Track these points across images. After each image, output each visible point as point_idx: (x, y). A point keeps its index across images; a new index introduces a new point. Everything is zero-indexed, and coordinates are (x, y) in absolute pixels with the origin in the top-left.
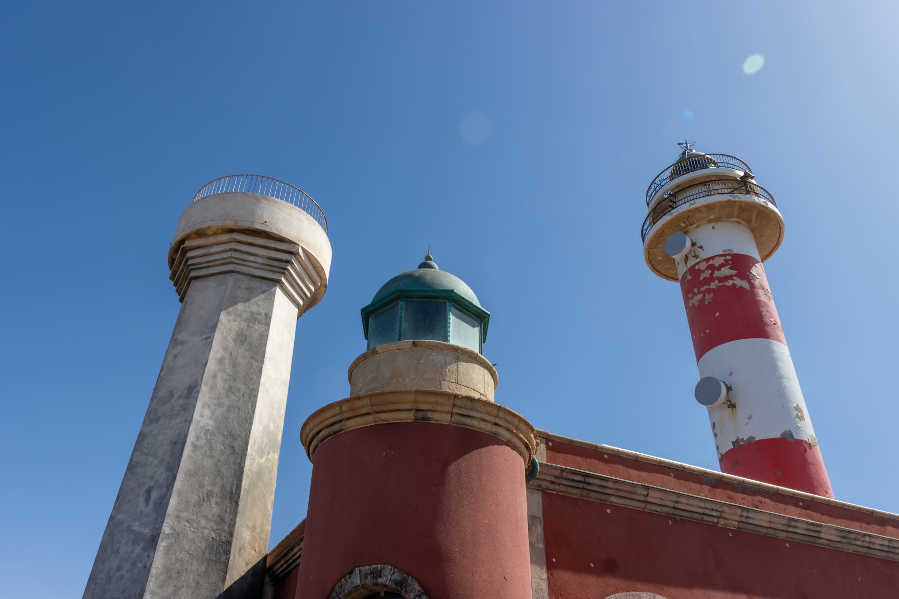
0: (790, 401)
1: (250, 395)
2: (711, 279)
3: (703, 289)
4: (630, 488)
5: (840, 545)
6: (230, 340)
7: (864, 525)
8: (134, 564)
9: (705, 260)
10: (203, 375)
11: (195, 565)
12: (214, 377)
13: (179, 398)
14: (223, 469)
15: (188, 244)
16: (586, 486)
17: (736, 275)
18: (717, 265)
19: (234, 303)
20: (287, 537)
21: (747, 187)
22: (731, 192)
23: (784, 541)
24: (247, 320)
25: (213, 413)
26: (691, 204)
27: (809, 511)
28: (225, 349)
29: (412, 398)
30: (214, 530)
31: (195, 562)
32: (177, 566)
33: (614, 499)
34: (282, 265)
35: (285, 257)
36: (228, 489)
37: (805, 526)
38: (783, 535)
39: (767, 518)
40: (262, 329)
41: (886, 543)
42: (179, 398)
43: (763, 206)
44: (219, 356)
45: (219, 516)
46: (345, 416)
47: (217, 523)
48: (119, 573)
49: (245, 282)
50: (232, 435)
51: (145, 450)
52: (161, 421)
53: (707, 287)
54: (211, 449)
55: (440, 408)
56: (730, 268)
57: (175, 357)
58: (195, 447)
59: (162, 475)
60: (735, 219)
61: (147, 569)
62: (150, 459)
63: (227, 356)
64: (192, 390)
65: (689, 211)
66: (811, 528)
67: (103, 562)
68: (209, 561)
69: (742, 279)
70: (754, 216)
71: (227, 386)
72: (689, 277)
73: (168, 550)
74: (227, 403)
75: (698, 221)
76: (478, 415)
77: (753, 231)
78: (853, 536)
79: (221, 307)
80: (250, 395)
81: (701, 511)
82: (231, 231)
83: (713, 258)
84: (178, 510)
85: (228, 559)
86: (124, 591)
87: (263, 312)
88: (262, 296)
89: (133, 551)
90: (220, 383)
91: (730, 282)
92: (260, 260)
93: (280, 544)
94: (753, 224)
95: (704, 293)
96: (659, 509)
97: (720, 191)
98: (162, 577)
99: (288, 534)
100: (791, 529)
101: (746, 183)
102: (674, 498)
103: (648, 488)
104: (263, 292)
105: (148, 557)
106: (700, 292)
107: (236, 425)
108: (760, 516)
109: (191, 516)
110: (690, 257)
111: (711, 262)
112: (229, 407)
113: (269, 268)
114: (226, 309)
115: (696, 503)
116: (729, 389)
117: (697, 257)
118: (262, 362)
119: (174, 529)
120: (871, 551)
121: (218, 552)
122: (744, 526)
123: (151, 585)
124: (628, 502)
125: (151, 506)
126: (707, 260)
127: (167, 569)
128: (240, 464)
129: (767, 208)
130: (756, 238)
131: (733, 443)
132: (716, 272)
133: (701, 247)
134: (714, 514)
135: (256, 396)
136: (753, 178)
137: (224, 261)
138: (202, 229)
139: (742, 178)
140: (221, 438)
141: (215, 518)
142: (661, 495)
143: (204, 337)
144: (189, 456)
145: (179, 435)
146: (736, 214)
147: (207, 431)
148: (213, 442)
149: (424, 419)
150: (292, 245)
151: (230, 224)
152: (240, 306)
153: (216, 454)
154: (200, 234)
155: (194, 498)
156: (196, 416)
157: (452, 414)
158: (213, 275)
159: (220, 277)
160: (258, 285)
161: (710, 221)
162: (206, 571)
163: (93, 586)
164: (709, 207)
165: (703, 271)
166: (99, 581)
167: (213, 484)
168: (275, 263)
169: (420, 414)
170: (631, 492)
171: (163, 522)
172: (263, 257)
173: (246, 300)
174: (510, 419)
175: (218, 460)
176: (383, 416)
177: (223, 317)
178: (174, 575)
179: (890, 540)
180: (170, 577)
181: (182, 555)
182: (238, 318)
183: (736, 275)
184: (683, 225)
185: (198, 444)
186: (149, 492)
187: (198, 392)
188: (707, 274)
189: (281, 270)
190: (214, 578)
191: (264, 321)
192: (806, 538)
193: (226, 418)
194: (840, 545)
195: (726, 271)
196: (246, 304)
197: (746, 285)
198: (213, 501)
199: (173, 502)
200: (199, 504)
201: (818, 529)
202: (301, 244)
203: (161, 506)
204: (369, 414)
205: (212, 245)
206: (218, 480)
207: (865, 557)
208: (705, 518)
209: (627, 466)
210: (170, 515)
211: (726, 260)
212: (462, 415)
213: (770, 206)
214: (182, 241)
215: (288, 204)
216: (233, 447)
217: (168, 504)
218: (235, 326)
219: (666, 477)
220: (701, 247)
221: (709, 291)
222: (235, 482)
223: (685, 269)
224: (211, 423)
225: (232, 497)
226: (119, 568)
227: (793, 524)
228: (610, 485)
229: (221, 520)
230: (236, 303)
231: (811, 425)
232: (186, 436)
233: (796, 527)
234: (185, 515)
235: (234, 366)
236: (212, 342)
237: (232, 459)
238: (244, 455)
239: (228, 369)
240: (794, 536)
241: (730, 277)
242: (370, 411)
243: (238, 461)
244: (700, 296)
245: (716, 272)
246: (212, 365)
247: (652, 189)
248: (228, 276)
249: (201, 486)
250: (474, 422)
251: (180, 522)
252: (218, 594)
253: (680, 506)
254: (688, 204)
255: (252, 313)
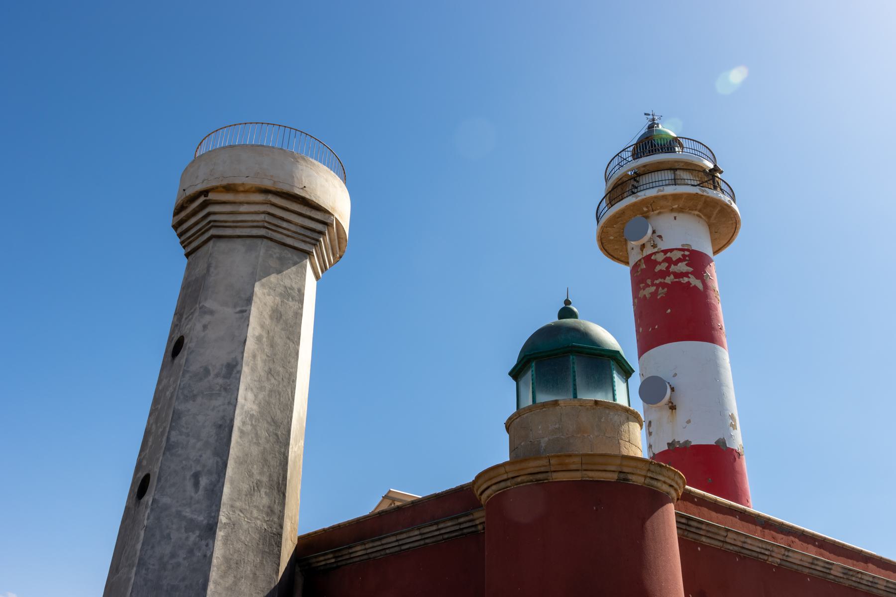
0: (727, 410)
1: (289, 379)
2: (664, 274)
3: (657, 282)
4: (716, 530)
5: (841, 580)
6: (267, 316)
7: (855, 562)
8: (191, 552)
9: (663, 251)
10: (243, 353)
11: (251, 557)
12: (254, 357)
13: (217, 375)
14: (269, 458)
15: (212, 196)
16: (688, 528)
17: (692, 273)
18: (674, 259)
19: (267, 274)
20: (324, 530)
21: (714, 182)
22: (698, 185)
23: (807, 576)
24: (281, 295)
25: (256, 396)
26: (659, 191)
27: (822, 550)
28: (262, 327)
29: (618, 462)
30: (266, 521)
31: (251, 553)
32: (236, 556)
33: (704, 539)
34: (315, 235)
35: (319, 227)
36: (275, 479)
37: (885, 584)
38: (806, 571)
39: (799, 557)
40: (296, 307)
41: (871, 579)
42: (217, 375)
43: (727, 205)
44: (257, 334)
45: (269, 507)
46: (553, 469)
47: (268, 515)
48: (173, 561)
49: (277, 250)
50: (274, 422)
51: (184, 430)
52: (199, 400)
53: (662, 280)
54: (257, 436)
55: (638, 472)
56: (687, 265)
57: (205, 327)
58: (242, 432)
59: (208, 458)
60: (697, 213)
61: (207, 559)
62: (192, 441)
63: (265, 334)
64: (232, 370)
65: (656, 197)
66: (827, 566)
67: (153, 547)
68: (263, 552)
69: (697, 278)
70: (715, 213)
71: (266, 369)
72: (644, 266)
73: (226, 539)
74: (268, 386)
75: (661, 208)
76: (663, 479)
77: (710, 226)
78: (851, 573)
79: (254, 278)
80: (289, 379)
81: (758, 550)
82: (266, 191)
83: (671, 250)
84: (232, 499)
85: (280, 551)
86: (183, 579)
87: (295, 286)
88: (294, 269)
89: (187, 538)
90: (260, 364)
91: (686, 280)
92: (293, 228)
93: (309, 535)
94: (712, 220)
95: (658, 286)
96: (731, 548)
97: (689, 182)
98: (223, 568)
99: (326, 526)
100: (813, 567)
101: (714, 177)
102: (743, 539)
103: (728, 530)
104: (295, 264)
105: (207, 545)
106: (653, 285)
107: (278, 412)
108: (796, 556)
109: (244, 506)
110: (648, 246)
111: (669, 255)
112: (271, 391)
113: (301, 237)
114: (260, 280)
115: (757, 544)
116: (673, 389)
117: (654, 246)
118: (298, 344)
119: (230, 519)
120: (860, 586)
121: (270, 544)
122: (784, 563)
123: (214, 575)
124: (713, 542)
125: (201, 492)
126: (665, 252)
127: (227, 560)
128: (284, 454)
129: (730, 207)
130: (711, 233)
131: (668, 444)
132: (673, 266)
133: (660, 237)
134: (767, 553)
135: (294, 381)
136: (721, 172)
137: (255, 224)
138: (234, 185)
139: (711, 170)
140: (266, 425)
141: (266, 509)
142: (735, 536)
143: (238, 309)
144: (237, 442)
145: (223, 418)
146: (699, 207)
147: (252, 416)
148: (258, 428)
149: (625, 479)
150: (327, 215)
151: (267, 184)
152: (273, 278)
153: (262, 441)
154: (229, 188)
155: (245, 487)
156: (240, 399)
157: (645, 477)
158: (239, 237)
159: (248, 241)
160: (290, 255)
161: (672, 210)
162: (261, 563)
163: (144, 571)
164: (676, 197)
165: (660, 263)
166: (151, 567)
167: (261, 473)
168: (308, 233)
169: (622, 476)
170: (716, 534)
171: (218, 511)
172: (296, 224)
173: (279, 272)
174: (633, 463)
175: (265, 448)
176: (591, 474)
177: (258, 289)
178: (234, 566)
179: (874, 577)
180: (229, 568)
181: (239, 546)
182: (272, 292)
183: (692, 273)
184: (645, 209)
185: (244, 429)
186: (196, 477)
187: (240, 372)
188: (663, 267)
189: (313, 241)
190: (269, 570)
191: (297, 298)
192: (821, 574)
193: (269, 403)
194: (841, 580)
195: (682, 267)
196: (279, 276)
197: (700, 286)
198: (263, 490)
199: (227, 490)
200: (250, 494)
201: (830, 567)
202: (336, 215)
203: (214, 494)
204: (578, 470)
205: (241, 203)
206: (265, 470)
207: (855, 590)
208: (761, 556)
209: (710, 509)
210: (225, 504)
211: (684, 256)
212: (651, 478)
213: (734, 206)
214: (205, 192)
215: (325, 168)
216: (277, 435)
217: (222, 492)
218: (269, 300)
219: (734, 518)
220: (660, 237)
221: (664, 285)
222: (281, 472)
223: (640, 257)
224: (255, 407)
225: (280, 488)
226: (173, 555)
227: (816, 562)
228: (704, 527)
229: (271, 511)
230: (269, 274)
231: (740, 435)
232: (232, 420)
233: (817, 565)
234: (238, 504)
235: (272, 346)
236: (249, 317)
237: (277, 448)
238: (287, 444)
239: (267, 350)
240: (814, 572)
241: (686, 274)
242: (580, 468)
243: (283, 450)
244: (653, 289)
245: (673, 266)
246: (251, 345)
247: (616, 161)
248: (259, 241)
249: (251, 475)
250: (659, 484)
251: (234, 512)
252: (273, 586)
253: (746, 546)
254: (656, 189)
255: (285, 287)
